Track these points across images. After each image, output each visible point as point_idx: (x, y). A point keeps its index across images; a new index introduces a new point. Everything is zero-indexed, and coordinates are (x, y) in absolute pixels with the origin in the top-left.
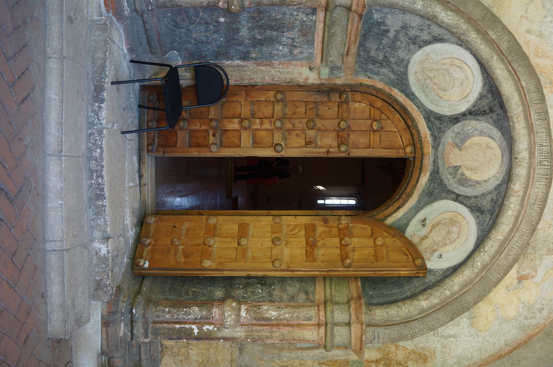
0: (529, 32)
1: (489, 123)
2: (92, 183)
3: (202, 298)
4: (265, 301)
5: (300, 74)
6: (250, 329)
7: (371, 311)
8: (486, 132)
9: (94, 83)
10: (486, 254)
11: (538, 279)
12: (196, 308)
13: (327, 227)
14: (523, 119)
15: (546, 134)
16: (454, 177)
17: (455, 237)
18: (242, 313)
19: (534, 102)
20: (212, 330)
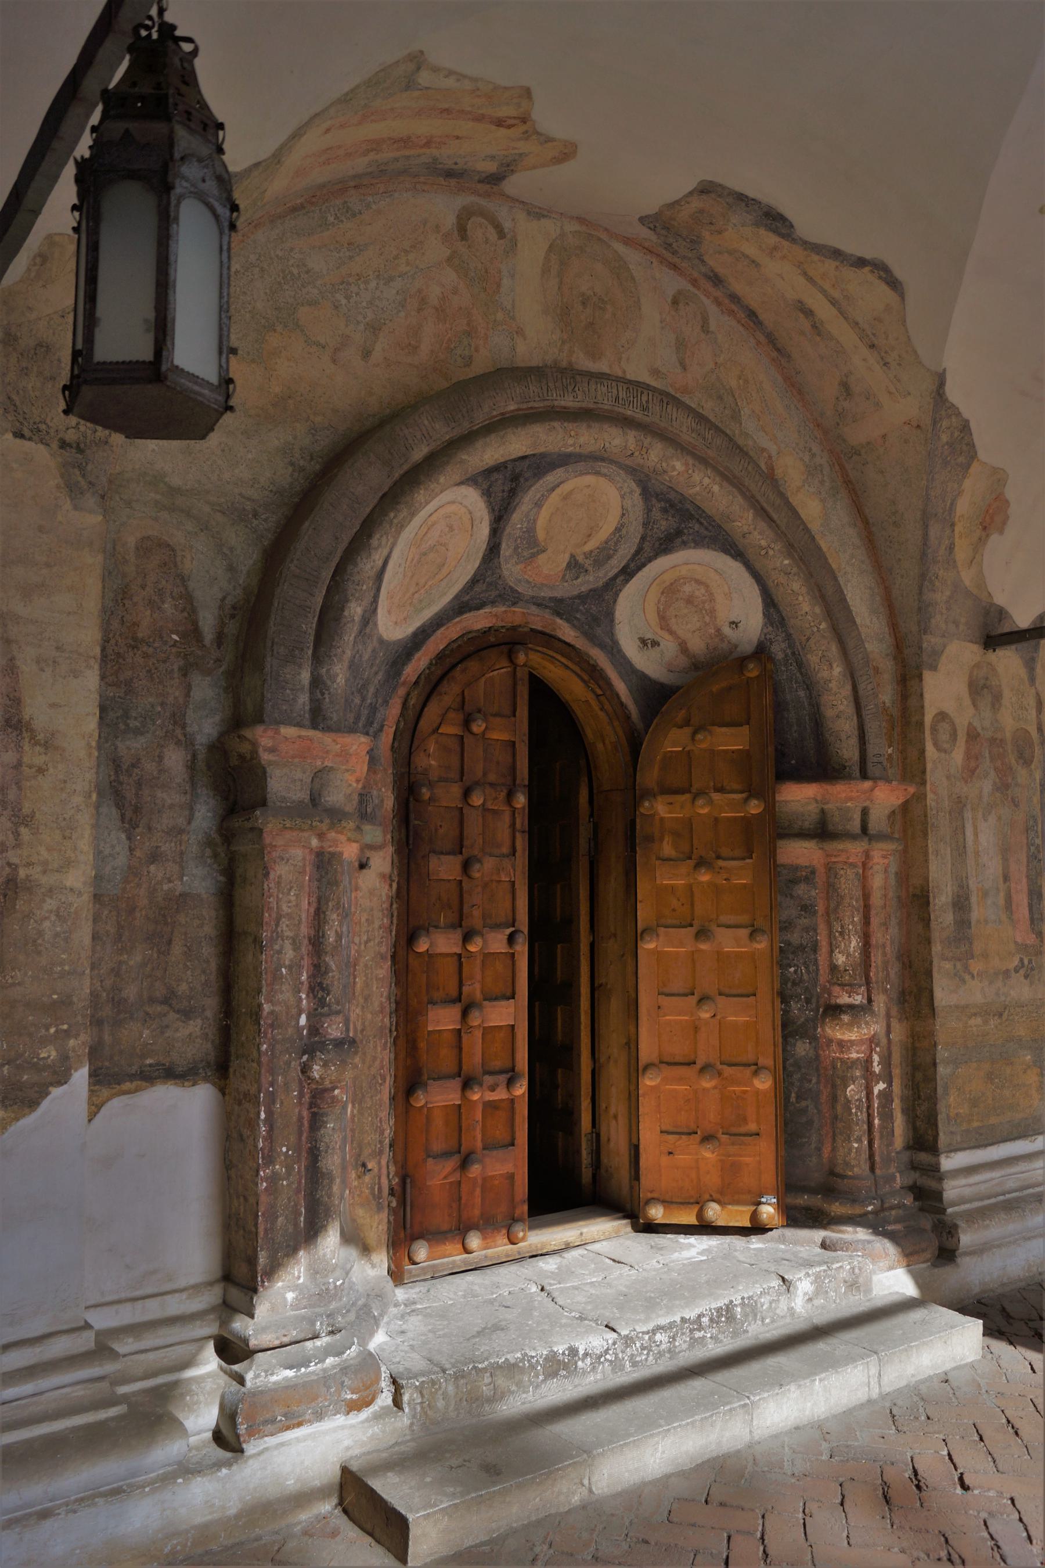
0: (366, 354)
1: (531, 486)
2: (711, 1338)
3: (814, 1080)
4: (816, 960)
5: (372, 892)
6: (875, 985)
7: (845, 767)
8: (542, 495)
9: (543, 1381)
10: (772, 545)
11: (773, 448)
12: (848, 1090)
13: (661, 840)
14: (575, 425)
15: (599, 385)
16: (586, 571)
17: (703, 591)
18: (857, 1003)
19: (545, 394)
20: (879, 1056)
